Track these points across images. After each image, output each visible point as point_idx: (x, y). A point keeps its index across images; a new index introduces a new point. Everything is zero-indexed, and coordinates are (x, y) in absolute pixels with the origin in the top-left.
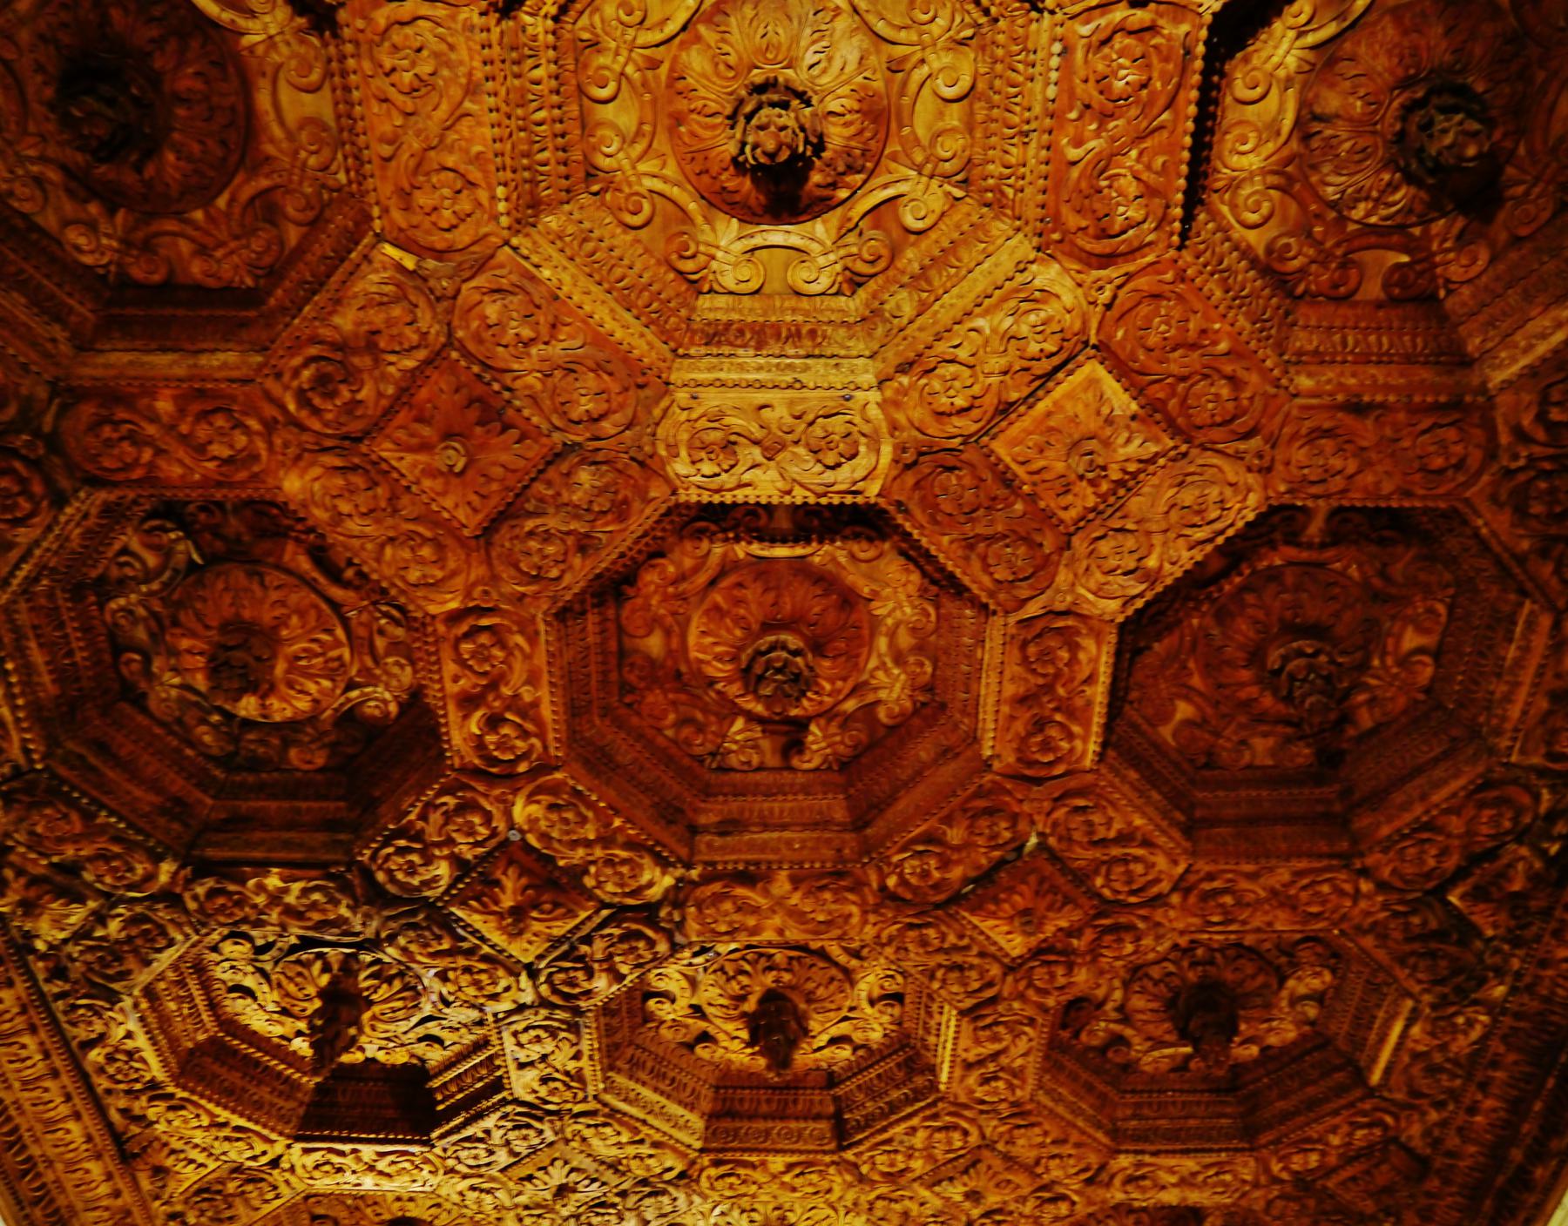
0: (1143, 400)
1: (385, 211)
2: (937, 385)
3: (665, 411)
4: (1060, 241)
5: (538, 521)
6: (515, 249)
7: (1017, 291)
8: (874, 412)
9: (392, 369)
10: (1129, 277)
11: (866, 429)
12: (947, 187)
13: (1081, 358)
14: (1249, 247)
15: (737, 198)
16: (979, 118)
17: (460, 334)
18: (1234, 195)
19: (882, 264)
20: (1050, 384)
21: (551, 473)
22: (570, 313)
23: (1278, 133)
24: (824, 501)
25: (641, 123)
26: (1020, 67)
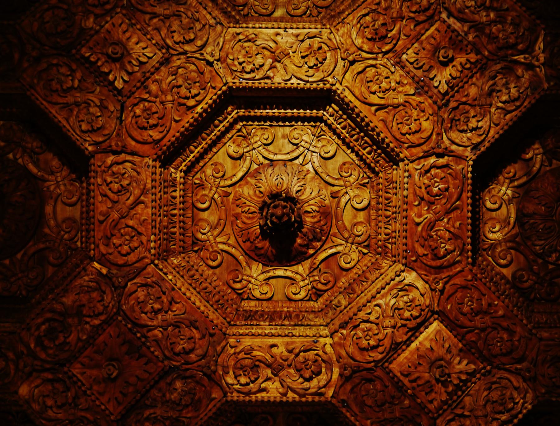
0: (464, 342)
1: (97, 246)
2: (360, 334)
3: (224, 348)
4: (415, 261)
5: (152, 411)
6: (156, 265)
7: (397, 285)
8: (329, 349)
9: (87, 326)
10: (450, 278)
11: (325, 357)
12: (360, 248)
13: (432, 320)
14: (504, 275)
15: (262, 252)
16: (373, 217)
17: (124, 307)
18: (494, 251)
19: (329, 286)
20: (417, 334)
21: (162, 384)
22: (180, 297)
23: (509, 223)
24: (304, 399)
25: (220, 219)
26: (390, 191)
